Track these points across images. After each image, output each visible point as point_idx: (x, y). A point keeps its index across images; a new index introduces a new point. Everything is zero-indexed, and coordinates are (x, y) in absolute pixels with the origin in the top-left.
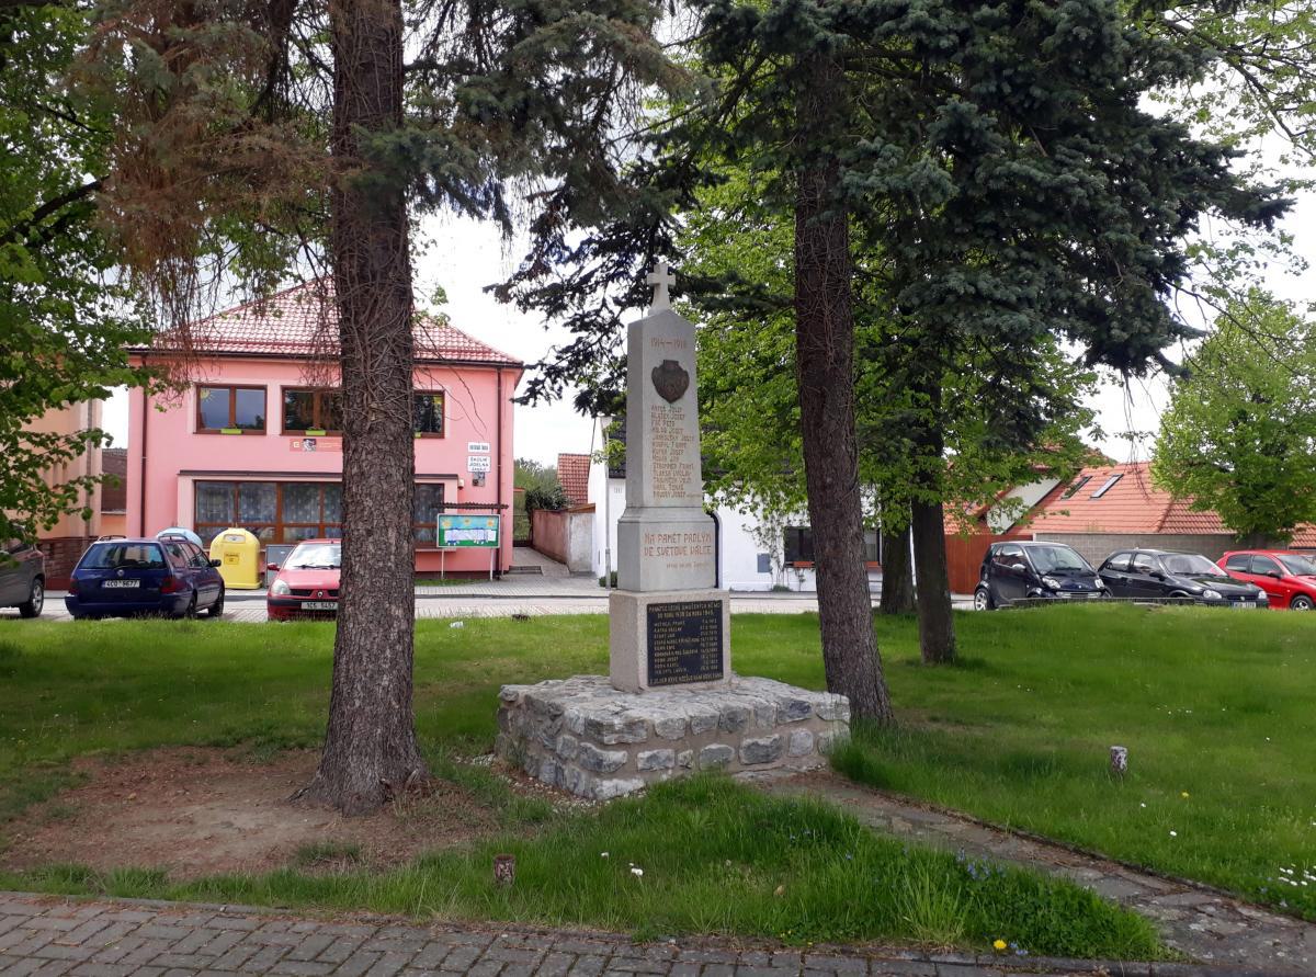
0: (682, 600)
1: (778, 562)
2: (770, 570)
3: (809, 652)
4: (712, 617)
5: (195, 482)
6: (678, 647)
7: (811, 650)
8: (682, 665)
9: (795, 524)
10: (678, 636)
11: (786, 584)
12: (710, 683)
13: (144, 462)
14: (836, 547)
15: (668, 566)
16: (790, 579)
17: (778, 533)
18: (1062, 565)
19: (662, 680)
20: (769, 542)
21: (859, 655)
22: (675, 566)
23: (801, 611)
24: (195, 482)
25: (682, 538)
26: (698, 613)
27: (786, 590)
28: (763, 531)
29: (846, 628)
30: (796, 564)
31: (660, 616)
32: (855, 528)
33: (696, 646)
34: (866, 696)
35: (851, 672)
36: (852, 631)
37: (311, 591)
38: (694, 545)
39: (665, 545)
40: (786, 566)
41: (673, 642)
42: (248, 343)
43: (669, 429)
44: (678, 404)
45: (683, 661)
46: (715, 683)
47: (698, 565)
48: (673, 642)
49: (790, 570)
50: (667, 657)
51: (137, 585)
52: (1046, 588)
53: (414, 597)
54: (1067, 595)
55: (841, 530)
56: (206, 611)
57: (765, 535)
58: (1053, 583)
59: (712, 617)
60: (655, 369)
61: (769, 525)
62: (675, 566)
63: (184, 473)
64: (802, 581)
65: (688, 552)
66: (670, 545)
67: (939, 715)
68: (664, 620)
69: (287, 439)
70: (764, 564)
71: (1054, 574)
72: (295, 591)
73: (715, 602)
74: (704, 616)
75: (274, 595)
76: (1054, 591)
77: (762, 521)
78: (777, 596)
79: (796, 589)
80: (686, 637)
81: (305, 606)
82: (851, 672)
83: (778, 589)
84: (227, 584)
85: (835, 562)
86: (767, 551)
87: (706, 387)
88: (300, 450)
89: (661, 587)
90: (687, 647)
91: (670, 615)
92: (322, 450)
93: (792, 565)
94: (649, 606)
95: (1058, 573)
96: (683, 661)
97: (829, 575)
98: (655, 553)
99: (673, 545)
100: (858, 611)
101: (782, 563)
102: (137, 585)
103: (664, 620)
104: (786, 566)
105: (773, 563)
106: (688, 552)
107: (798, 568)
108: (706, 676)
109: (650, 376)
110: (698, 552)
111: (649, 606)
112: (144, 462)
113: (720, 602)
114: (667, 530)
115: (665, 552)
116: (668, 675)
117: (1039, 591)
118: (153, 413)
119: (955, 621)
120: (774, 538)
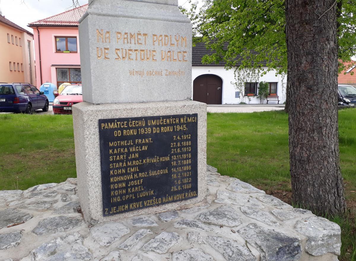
0: (149, 114)
1: (242, 94)
2: (239, 97)
3: (259, 131)
4: (185, 133)
5: (56, 68)
6: (142, 169)
7: (282, 162)
9: (249, 81)
10: (143, 155)
11: (244, 102)
12: (183, 203)
13: (40, 62)
14: (313, 61)
15: (132, 73)
16: (246, 100)
17: (243, 84)
18: (350, 93)
19: (121, 208)
20: (239, 88)
21: (325, 158)
22: (140, 73)
23: (252, 112)
25: (149, 40)
26: (168, 129)
27: (245, 103)
28: (238, 84)
29: (316, 135)
30: (248, 95)
32: (332, 43)
33: (167, 165)
34: (328, 193)
35: (316, 172)
37: (67, 103)
38: (165, 48)
39: (127, 46)
40: (245, 95)
41: (137, 163)
42: (70, 22)
45: (148, 183)
46: (188, 202)
47: (170, 74)
48: (137, 163)
49: (246, 97)
50: (127, 182)
51: (4, 100)
52: (345, 102)
54: (353, 105)
55: (319, 46)
56: (41, 110)
57: (238, 85)
58: (347, 100)
59: (185, 133)
61: (240, 82)
62: (140, 73)
63: (53, 65)
64: (250, 100)
65: (158, 56)
66: (133, 47)
68: (123, 138)
70: (237, 95)
71: (348, 97)
72: (61, 103)
73: (189, 116)
75: (55, 104)
76: (348, 103)
77: (237, 80)
78: (242, 105)
79: (248, 103)
80: (152, 156)
81: (65, 108)
82: (316, 172)
83: (242, 103)
84: (49, 101)
85: (310, 76)
86: (239, 91)
89: (122, 99)
90: (152, 167)
93: (247, 95)
94: (101, 122)
95: (348, 97)
96: (148, 183)
97: (303, 88)
98: (112, 55)
99: (138, 47)
100: (328, 121)
101: (244, 94)
102: (4, 100)
104: (245, 95)
105: (240, 95)
106: (158, 56)
107: (249, 96)
108: (179, 196)
110: (170, 58)
111: (101, 122)
112: (40, 62)
113: (196, 115)
114: (131, 27)
116: (130, 201)
117: (342, 103)
120: (241, 86)
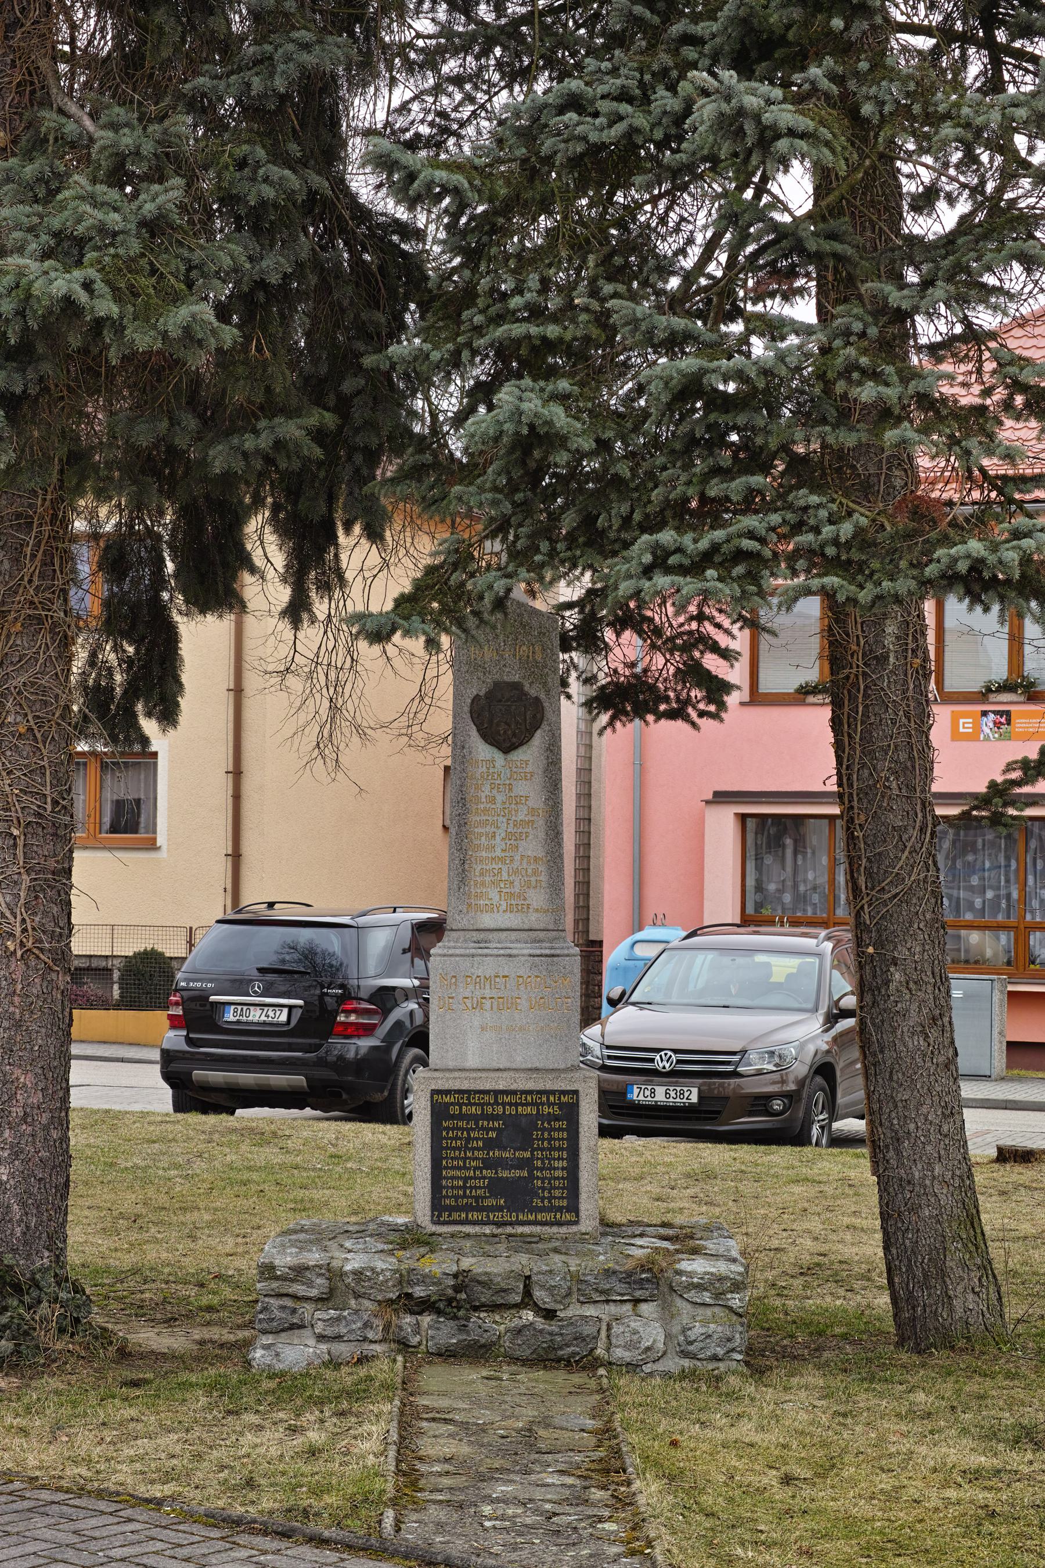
4: (557, 1119)
5: (743, 818)
6: (488, 1164)
8: (493, 1194)
10: (489, 1144)
24: (743, 818)
31: (454, 1110)
33: (522, 1164)
36: (901, 1165)
39: (478, 994)
43: (500, 798)
44: (521, 755)
45: (496, 1187)
50: (466, 1179)
53: (963, 1104)
60: (476, 699)
63: (721, 798)
66: (487, 993)
68: (461, 1117)
88: (973, 737)
96: (496, 1187)
103: (461, 1117)
111: (434, 1092)
113: (576, 1092)
115: (479, 1006)
116: (468, 1208)
118: (763, 646)
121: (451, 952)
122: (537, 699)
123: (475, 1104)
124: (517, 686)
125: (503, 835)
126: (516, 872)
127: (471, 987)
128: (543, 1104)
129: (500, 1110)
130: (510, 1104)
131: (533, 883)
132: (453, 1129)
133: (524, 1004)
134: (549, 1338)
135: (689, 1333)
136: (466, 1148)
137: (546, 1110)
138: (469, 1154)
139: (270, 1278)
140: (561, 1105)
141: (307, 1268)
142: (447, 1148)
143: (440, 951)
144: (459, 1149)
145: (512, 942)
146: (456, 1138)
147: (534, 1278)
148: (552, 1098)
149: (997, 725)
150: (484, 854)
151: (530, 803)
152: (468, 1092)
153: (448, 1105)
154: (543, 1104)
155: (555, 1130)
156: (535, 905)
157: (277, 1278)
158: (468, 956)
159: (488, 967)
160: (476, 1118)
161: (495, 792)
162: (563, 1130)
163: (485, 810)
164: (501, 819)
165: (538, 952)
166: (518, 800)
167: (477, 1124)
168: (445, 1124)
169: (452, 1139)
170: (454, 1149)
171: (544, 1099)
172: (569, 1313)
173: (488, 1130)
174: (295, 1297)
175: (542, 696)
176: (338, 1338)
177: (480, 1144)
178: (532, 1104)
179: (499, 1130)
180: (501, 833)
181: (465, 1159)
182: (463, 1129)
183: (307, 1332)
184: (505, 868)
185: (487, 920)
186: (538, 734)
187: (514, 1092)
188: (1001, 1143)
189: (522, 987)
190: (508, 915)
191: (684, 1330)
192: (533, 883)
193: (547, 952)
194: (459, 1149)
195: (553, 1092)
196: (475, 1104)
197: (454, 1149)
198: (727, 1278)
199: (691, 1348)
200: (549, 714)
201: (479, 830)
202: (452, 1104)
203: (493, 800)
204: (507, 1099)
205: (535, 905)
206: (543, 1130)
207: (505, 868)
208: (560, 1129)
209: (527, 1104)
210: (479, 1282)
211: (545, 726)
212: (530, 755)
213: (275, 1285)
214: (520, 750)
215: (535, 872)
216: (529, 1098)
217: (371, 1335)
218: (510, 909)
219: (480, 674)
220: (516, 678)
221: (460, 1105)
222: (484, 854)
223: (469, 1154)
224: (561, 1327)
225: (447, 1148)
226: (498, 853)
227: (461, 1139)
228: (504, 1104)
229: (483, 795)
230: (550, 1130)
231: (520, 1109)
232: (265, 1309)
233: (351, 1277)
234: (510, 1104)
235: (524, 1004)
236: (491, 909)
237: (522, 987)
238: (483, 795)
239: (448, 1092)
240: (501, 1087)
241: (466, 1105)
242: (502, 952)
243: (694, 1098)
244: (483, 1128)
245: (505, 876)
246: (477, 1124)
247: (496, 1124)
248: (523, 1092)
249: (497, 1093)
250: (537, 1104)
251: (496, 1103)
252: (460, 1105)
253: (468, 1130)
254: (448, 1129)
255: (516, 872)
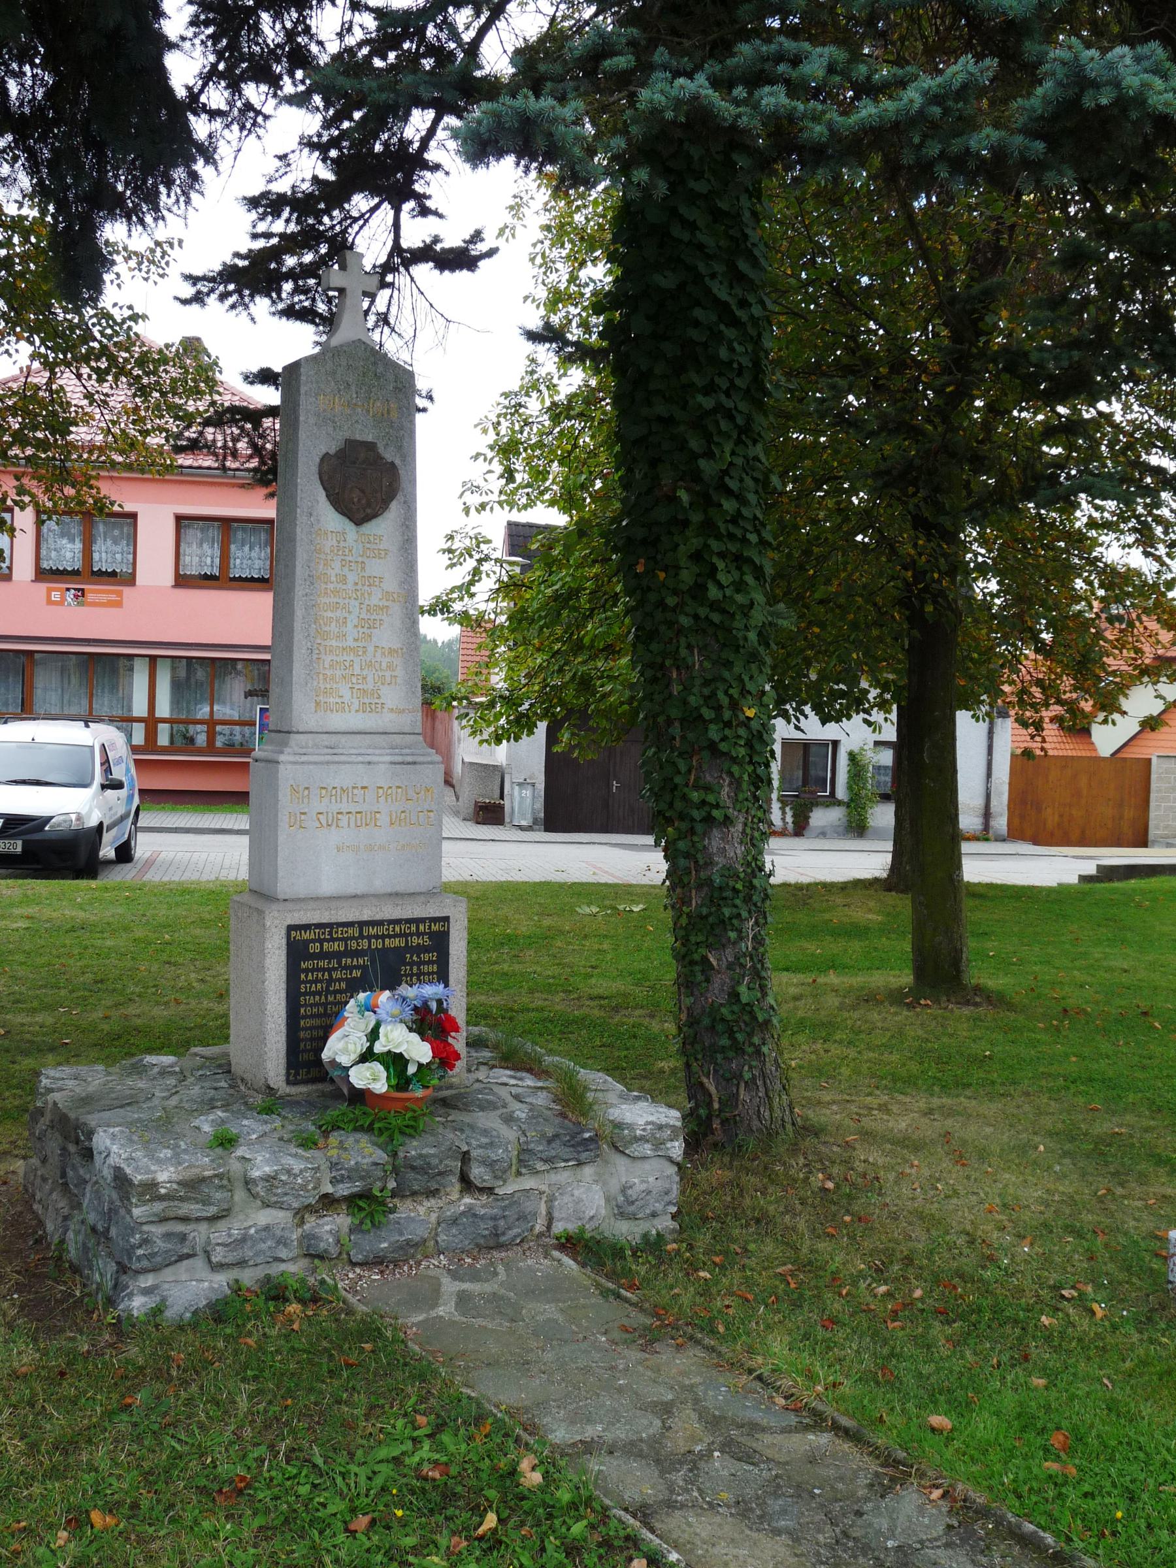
4: (426, 950)
31: (314, 948)
39: (335, 808)
43: (352, 578)
44: (371, 528)
60: (325, 458)
66: (344, 807)
67: (930, 1435)
68: (323, 955)
69: (43, 587)
73: (435, 920)
74: (408, 949)
87: (1145, 583)
88: (61, 603)
91: (336, 946)
92: (94, 604)
109: (315, 479)
111: (290, 928)
113: (446, 919)
115: (333, 822)
119: (968, 903)
121: (304, 758)
122: (392, 464)
123: (338, 939)
124: (371, 446)
125: (355, 622)
126: (370, 665)
127: (325, 800)
128: (411, 935)
129: (364, 944)
130: (377, 937)
131: (388, 679)
132: (313, 971)
133: (383, 819)
134: (491, 1223)
135: (630, 1192)
136: (328, 991)
137: (415, 941)
138: (331, 998)
139: (151, 1200)
140: (432, 935)
141: (203, 1180)
142: (305, 994)
143: (292, 758)
144: (319, 993)
145: (369, 747)
146: (316, 981)
147: (474, 1154)
148: (421, 927)
149: (76, 596)
150: (334, 643)
151: (385, 586)
152: (330, 925)
153: (307, 943)
154: (411, 935)
155: (424, 963)
156: (390, 704)
157: (161, 1198)
158: (321, 763)
159: (343, 777)
160: (338, 955)
161: (346, 569)
162: (433, 962)
163: (336, 592)
164: (353, 602)
165: (400, 759)
166: (371, 581)
167: (339, 963)
168: (303, 966)
169: (311, 982)
170: (314, 994)
171: (414, 928)
172: (509, 1189)
173: (351, 968)
174: (185, 1219)
175: (397, 462)
176: (242, 1263)
177: (343, 985)
178: (400, 935)
179: (363, 968)
180: (352, 620)
181: (325, 1005)
182: (324, 970)
183: (199, 1263)
184: (357, 660)
185: (337, 721)
186: (394, 505)
187: (380, 923)
188: (129, 865)
189: (382, 799)
190: (360, 715)
191: (624, 1190)
192: (388, 679)
193: (409, 759)
194: (319, 993)
195: (422, 920)
196: (338, 939)
197: (314, 994)
198: (667, 1126)
199: (632, 1209)
200: (404, 484)
201: (329, 614)
202: (313, 941)
203: (344, 580)
204: (373, 931)
205: (390, 704)
206: (412, 964)
207: (357, 660)
208: (430, 962)
209: (395, 936)
210: (413, 1168)
211: (400, 497)
212: (384, 527)
213: (158, 1207)
214: (374, 522)
215: (390, 667)
216: (397, 929)
217: (283, 1253)
218: (364, 708)
219: (330, 429)
220: (370, 438)
221: (321, 941)
222: (334, 643)
223: (331, 998)
224: (504, 1209)
225: (305, 994)
226: (350, 643)
227: (321, 981)
228: (369, 937)
229: (333, 573)
230: (419, 964)
231: (387, 941)
232: (145, 1242)
233: (261, 1184)
234: (377, 937)
235: (383, 819)
236: (342, 708)
237: (382, 799)
238: (333, 573)
239: (306, 927)
240: (365, 918)
241: (328, 941)
242: (360, 759)
243: (19, 849)
244: (346, 967)
245: (357, 671)
246: (339, 963)
247: (361, 961)
248: (409, 921)
249: (362, 924)
250: (405, 935)
251: (361, 936)
252: (321, 941)
253: (330, 970)
254: (307, 971)
255: (370, 665)
